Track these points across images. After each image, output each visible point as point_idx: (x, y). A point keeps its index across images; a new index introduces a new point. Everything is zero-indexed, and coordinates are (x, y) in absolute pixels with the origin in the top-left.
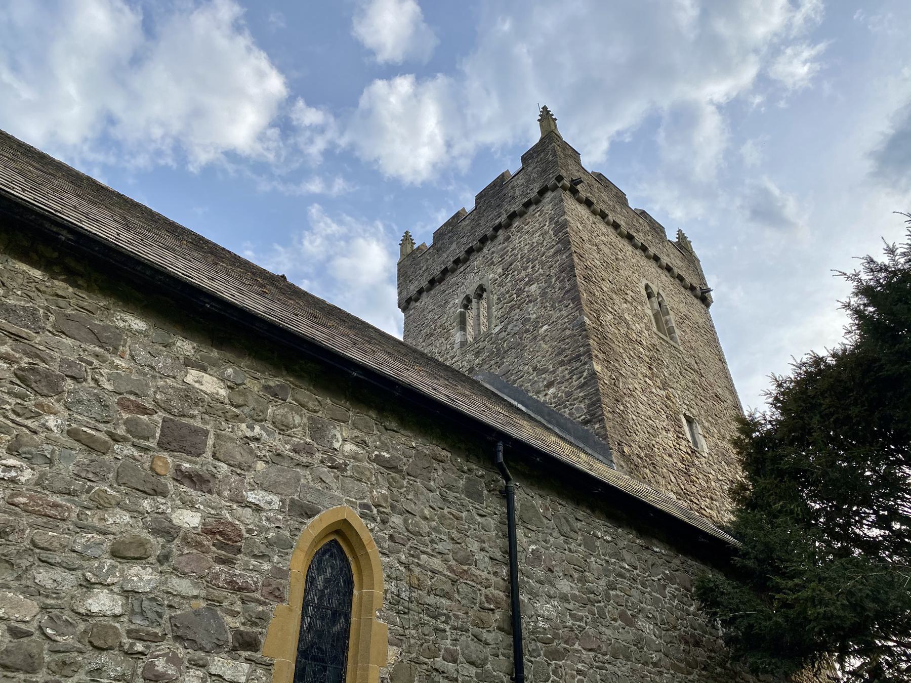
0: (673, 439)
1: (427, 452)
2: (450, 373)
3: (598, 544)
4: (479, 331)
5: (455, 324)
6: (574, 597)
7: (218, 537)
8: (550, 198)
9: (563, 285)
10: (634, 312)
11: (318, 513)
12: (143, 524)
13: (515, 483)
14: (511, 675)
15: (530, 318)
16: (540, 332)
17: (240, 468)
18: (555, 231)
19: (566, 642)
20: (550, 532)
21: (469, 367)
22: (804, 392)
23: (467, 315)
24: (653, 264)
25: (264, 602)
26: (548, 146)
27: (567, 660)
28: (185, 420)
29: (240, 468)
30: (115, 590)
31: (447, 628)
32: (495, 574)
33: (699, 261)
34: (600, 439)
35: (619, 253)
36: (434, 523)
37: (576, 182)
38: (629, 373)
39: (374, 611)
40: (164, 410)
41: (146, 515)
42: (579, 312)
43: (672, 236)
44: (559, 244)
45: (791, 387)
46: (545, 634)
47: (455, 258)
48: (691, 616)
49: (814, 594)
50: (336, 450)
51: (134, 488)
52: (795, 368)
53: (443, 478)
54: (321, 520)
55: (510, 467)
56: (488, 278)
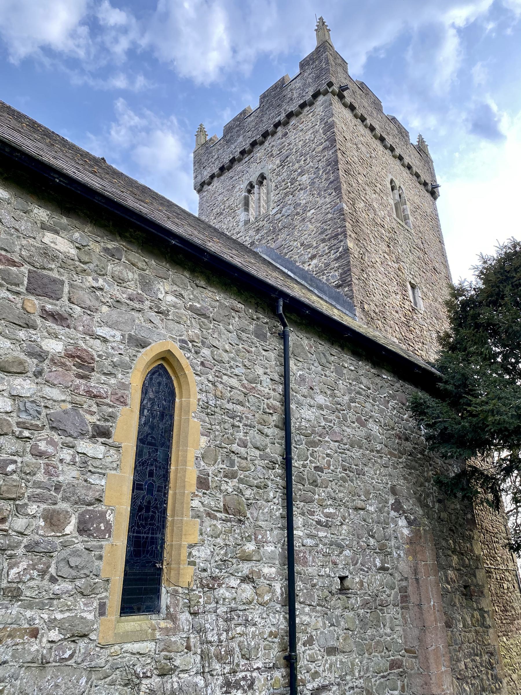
0: (400, 300)
1: (227, 305)
2: (238, 246)
3: (345, 372)
4: (260, 212)
5: (240, 206)
6: (327, 407)
7: (77, 359)
8: (322, 101)
9: (328, 176)
10: (380, 201)
11: (149, 344)
12: (21, 349)
13: (290, 329)
14: (283, 456)
15: (301, 203)
16: (308, 215)
17: (89, 310)
18: (325, 130)
19: (320, 436)
20: (312, 362)
21: (251, 241)
22: (502, 267)
23: (250, 198)
24: (398, 162)
25: (113, 406)
26: (322, 55)
27: (320, 447)
28: (45, 272)
29: (89, 310)
30: (5, 395)
31: (241, 425)
32: (274, 390)
33: (432, 162)
34: (348, 299)
35: (373, 152)
36: (232, 354)
37: (343, 89)
38: (373, 250)
39: (191, 412)
40: (29, 263)
41: (22, 342)
42: (340, 199)
43: (414, 140)
44: (327, 142)
45: (493, 264)
46: (306, 430)
47: (241, 149)
48: (405, 421)
49: (494, 407)
50: (161, 300)
51: (12, 322)
52: (498, 249)
53: (238, 323)
54: (151, 350)
55: (286, 316)
56: (268, 168)
